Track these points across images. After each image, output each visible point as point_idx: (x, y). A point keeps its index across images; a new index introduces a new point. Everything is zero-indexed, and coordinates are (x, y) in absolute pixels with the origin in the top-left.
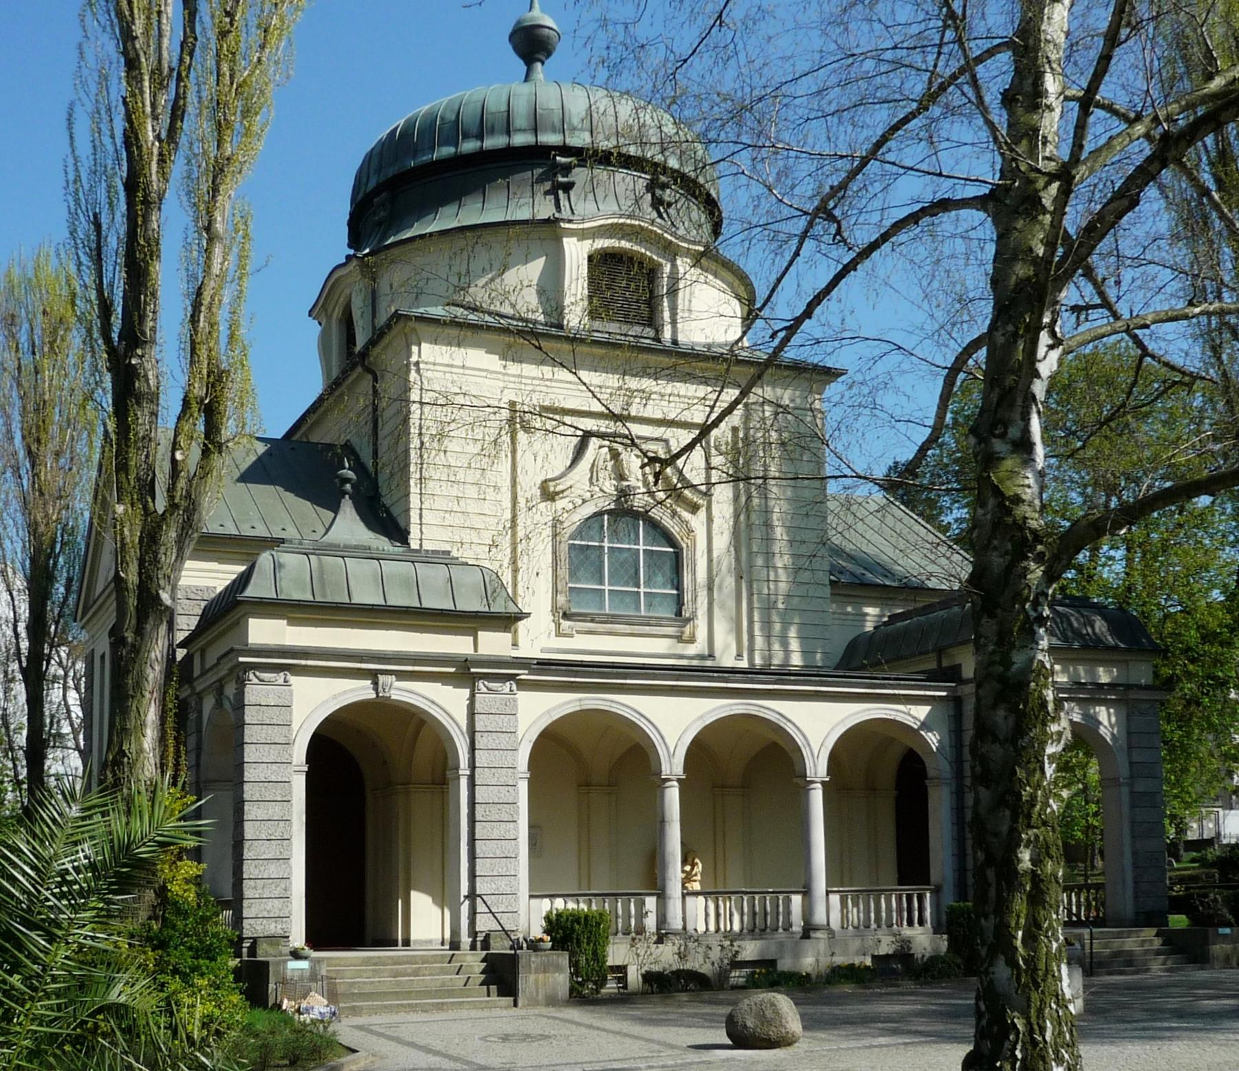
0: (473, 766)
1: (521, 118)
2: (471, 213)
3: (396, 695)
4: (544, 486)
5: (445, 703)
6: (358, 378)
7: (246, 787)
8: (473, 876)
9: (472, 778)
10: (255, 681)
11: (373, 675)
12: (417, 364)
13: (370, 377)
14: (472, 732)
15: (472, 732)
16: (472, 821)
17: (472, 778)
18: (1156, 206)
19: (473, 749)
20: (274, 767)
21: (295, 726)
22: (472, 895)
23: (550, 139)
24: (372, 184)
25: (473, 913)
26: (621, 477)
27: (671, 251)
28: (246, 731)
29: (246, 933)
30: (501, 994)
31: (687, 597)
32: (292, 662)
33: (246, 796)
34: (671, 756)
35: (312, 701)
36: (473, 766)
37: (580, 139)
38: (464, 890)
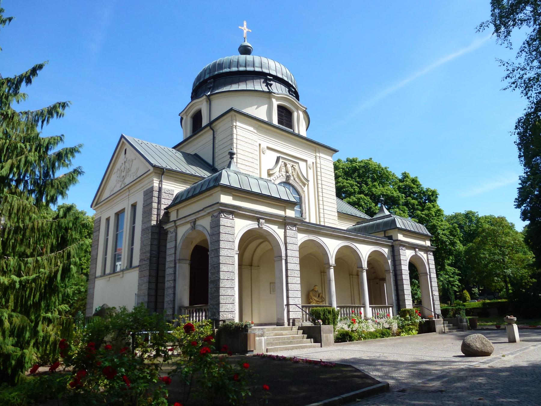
0: (286, 256)
1: (257, 64)
2: (242, 86)
3: (265, 228)
4: (269, 170)
5: (277, 232)
6: (208, 131)
7: (221, 258)
8: (288, 297)
9: (286, 260)
10: (223, 216)
11: (258, 219)
12: (236, 126)
13: (212, 132)
14: (286, 244)
15: (286, 244)
16: (287, 277)
17: (286, 260)
18: (232, 175)
19: (286, 249)
20: (229, 250)
21: (235, 235)
22: (288, 305)
23: (266, 71)
24: (207, 76)
25: (288, 312)
26: (287, 172)
27: (297, 108)
28: (221, 236)
29: (221, 318)
30: (315, 342)
31: (304, 212)
32: (234, 212)
33: (221, 262)
34: (332, 257)
35: (241, 226)
36: (286, 256)
37: (273, 73)
38: (285, 303)
